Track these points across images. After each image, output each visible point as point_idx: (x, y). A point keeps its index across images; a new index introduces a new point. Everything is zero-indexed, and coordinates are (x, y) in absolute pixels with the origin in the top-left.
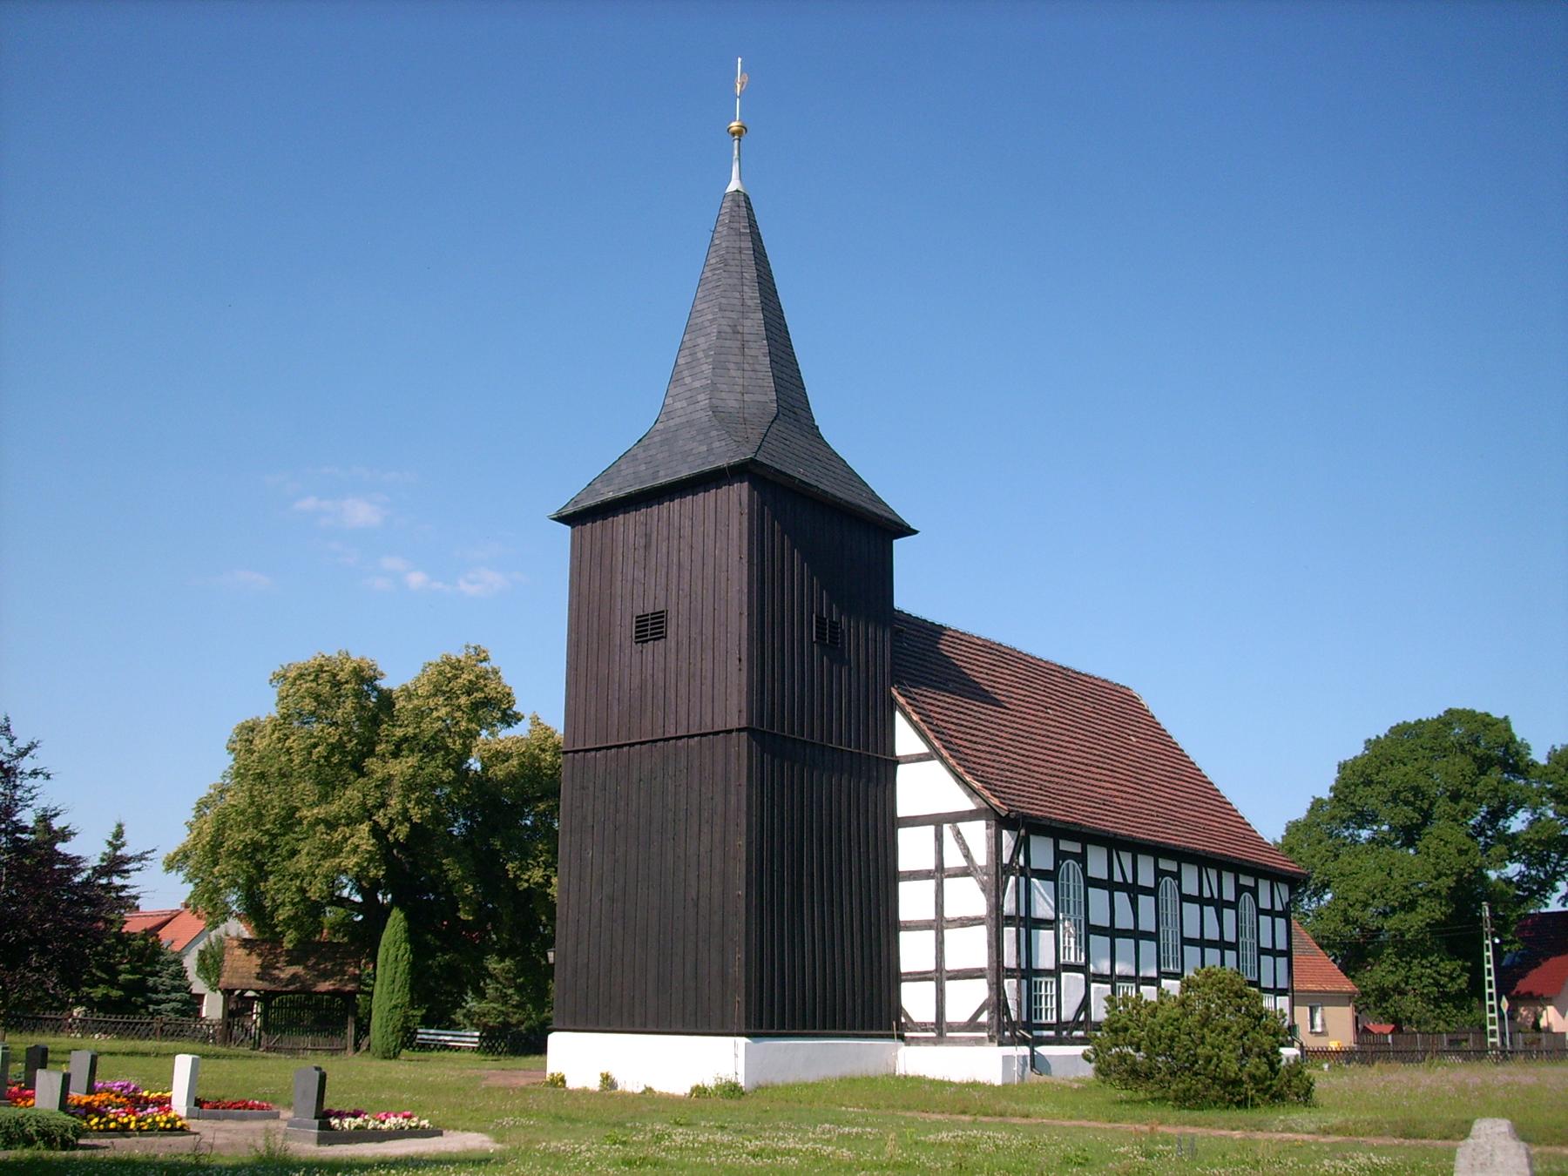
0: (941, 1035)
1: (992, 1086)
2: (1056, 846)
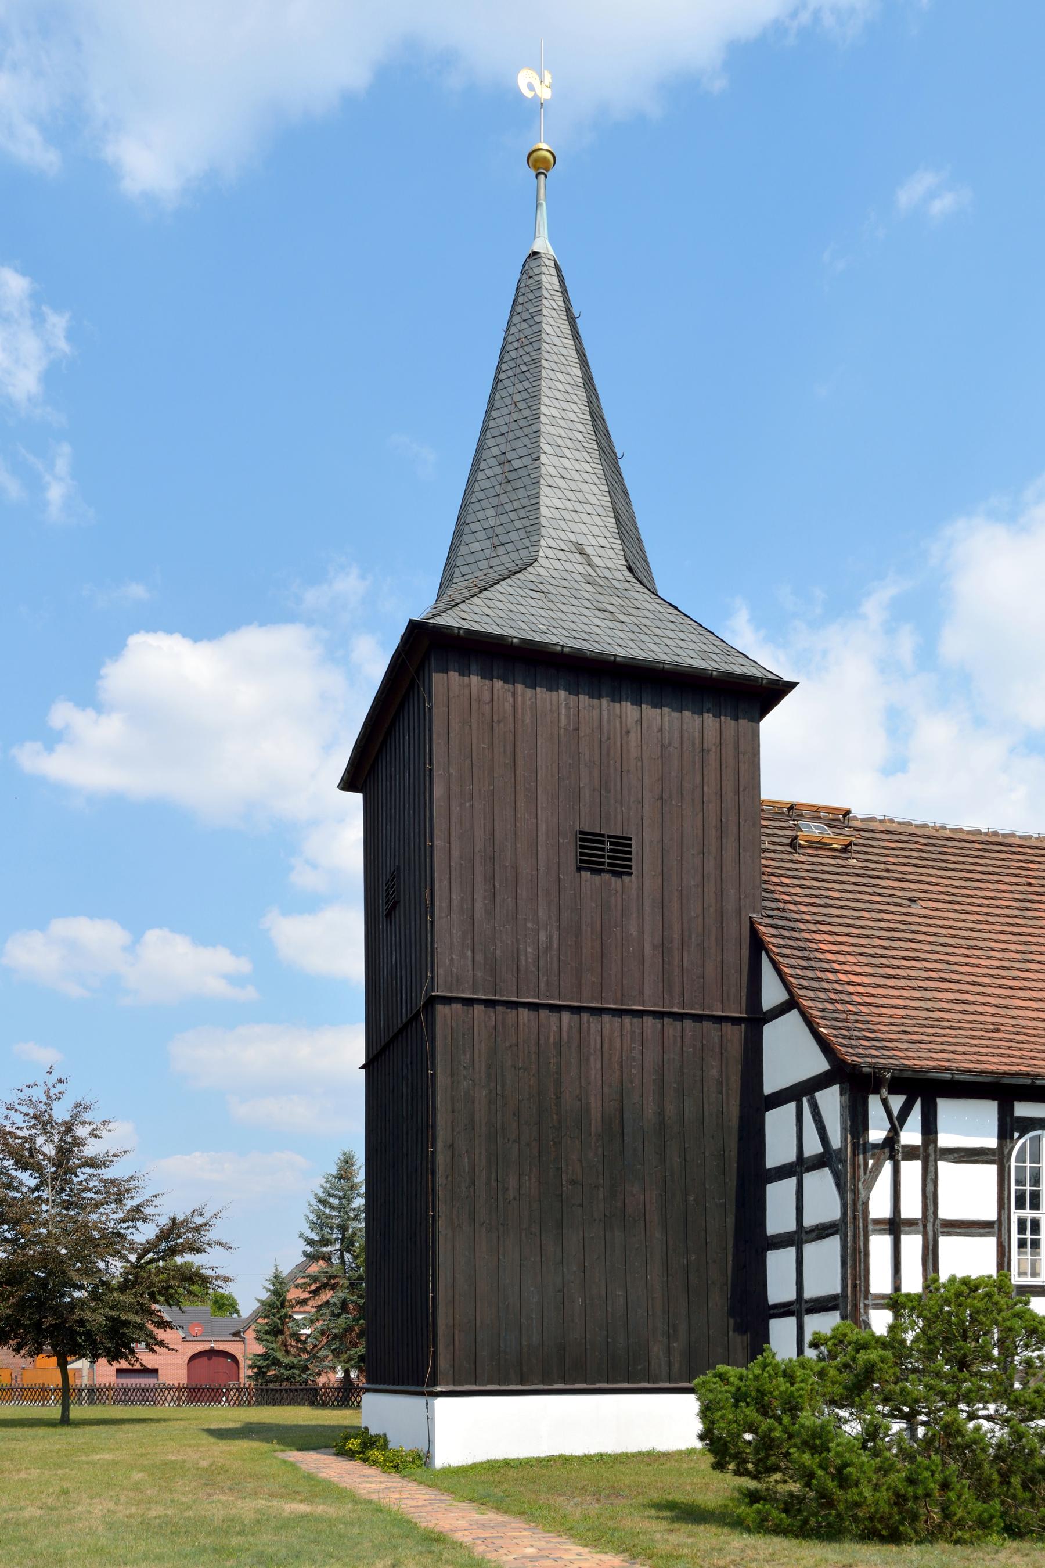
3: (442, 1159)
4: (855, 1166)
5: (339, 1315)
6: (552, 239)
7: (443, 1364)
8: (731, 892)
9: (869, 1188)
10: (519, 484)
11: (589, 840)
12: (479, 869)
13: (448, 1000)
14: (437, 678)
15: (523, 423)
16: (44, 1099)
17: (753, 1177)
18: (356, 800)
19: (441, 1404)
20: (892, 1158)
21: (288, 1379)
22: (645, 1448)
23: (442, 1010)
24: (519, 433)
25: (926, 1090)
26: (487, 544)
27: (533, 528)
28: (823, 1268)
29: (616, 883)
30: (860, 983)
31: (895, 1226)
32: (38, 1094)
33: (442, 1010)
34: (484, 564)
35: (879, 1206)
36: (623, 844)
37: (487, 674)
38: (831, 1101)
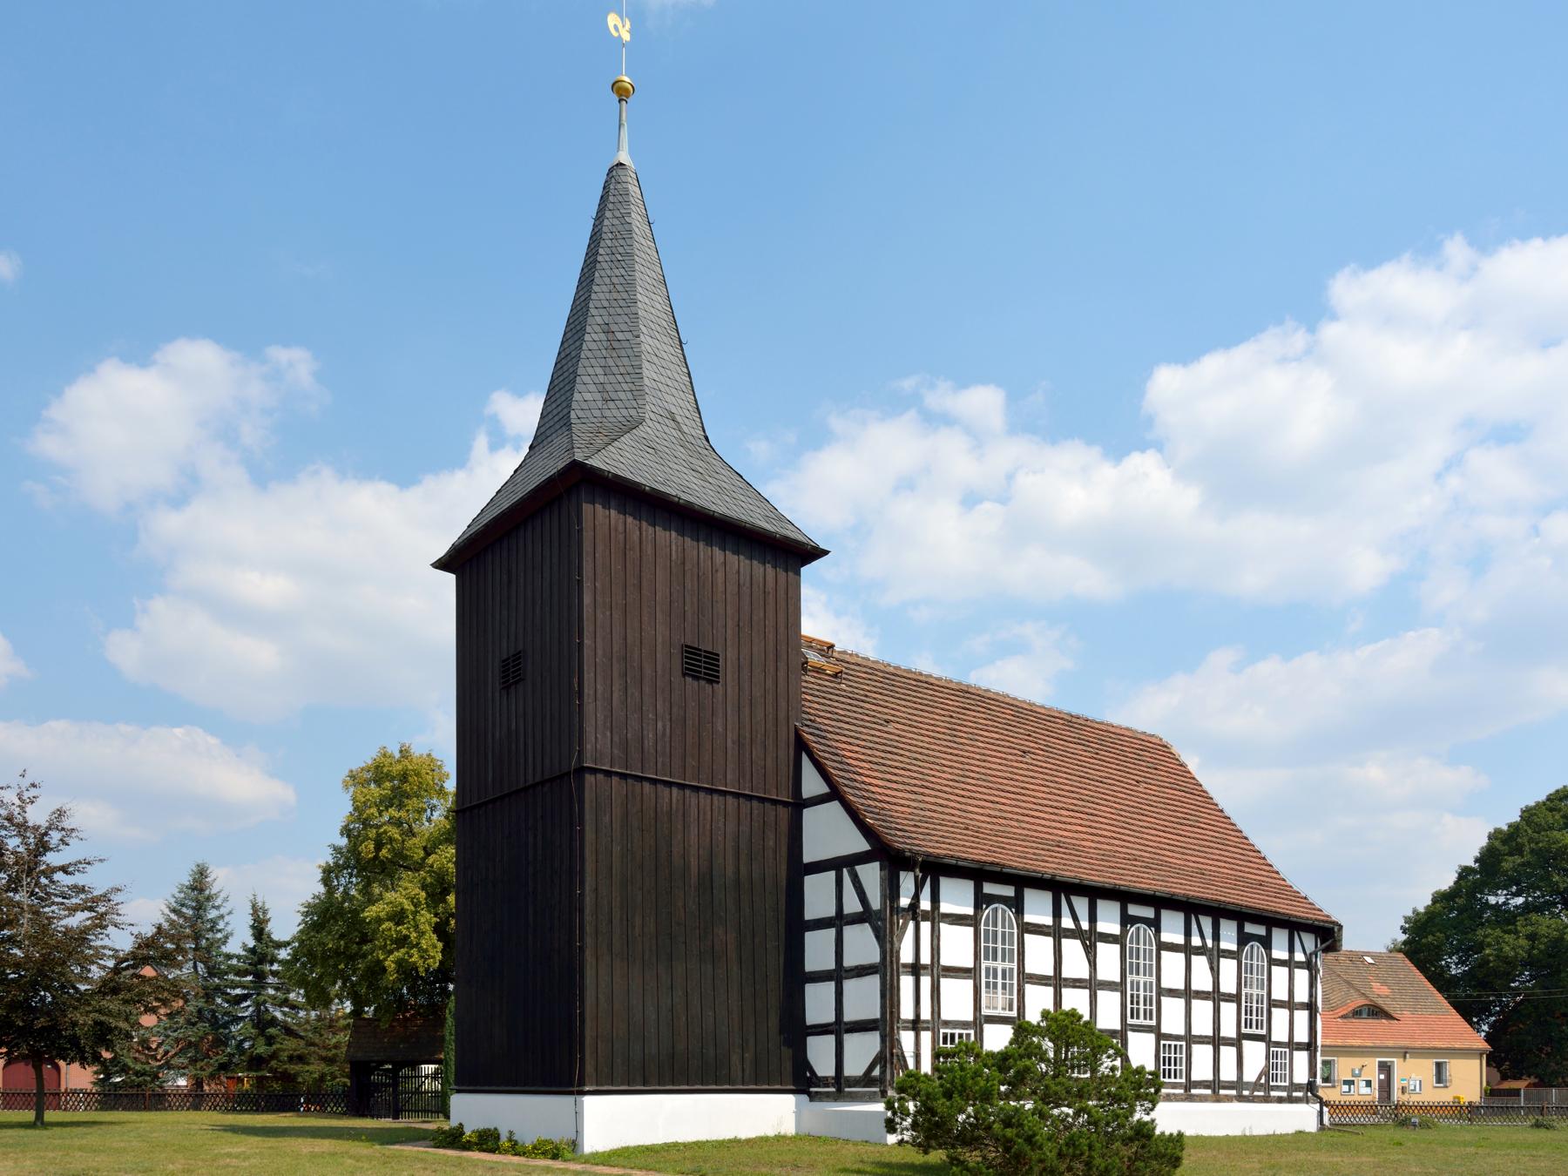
0: (839, 1090)
1: (780, 1138)
2: (1240, 929)
3: (589, 900)
5: (194, 1024)
6: (631, 153)
8: (783, 704)
9: (900, 941)
10: (623, 353)
11: (690, 652)
13: (594, 771)
15: (622, 303)
16: (18, 802)
17: (796, 926)
18: (450, 579)
19: (588, 1100)
20: (914, 918)
21: (139, 1086)
22: (729, 1135)
23: (589, 779)
24: (619, 311)
25: (935, 870)
26: (598, 396)
27: (638, 393)
28: (862, 999)
29: (708, 687)
31: (916, 969)
33: (589, 779)
35: (906, 956)
36: (713, 658)
37: (623, 511)
38: (871, 874)
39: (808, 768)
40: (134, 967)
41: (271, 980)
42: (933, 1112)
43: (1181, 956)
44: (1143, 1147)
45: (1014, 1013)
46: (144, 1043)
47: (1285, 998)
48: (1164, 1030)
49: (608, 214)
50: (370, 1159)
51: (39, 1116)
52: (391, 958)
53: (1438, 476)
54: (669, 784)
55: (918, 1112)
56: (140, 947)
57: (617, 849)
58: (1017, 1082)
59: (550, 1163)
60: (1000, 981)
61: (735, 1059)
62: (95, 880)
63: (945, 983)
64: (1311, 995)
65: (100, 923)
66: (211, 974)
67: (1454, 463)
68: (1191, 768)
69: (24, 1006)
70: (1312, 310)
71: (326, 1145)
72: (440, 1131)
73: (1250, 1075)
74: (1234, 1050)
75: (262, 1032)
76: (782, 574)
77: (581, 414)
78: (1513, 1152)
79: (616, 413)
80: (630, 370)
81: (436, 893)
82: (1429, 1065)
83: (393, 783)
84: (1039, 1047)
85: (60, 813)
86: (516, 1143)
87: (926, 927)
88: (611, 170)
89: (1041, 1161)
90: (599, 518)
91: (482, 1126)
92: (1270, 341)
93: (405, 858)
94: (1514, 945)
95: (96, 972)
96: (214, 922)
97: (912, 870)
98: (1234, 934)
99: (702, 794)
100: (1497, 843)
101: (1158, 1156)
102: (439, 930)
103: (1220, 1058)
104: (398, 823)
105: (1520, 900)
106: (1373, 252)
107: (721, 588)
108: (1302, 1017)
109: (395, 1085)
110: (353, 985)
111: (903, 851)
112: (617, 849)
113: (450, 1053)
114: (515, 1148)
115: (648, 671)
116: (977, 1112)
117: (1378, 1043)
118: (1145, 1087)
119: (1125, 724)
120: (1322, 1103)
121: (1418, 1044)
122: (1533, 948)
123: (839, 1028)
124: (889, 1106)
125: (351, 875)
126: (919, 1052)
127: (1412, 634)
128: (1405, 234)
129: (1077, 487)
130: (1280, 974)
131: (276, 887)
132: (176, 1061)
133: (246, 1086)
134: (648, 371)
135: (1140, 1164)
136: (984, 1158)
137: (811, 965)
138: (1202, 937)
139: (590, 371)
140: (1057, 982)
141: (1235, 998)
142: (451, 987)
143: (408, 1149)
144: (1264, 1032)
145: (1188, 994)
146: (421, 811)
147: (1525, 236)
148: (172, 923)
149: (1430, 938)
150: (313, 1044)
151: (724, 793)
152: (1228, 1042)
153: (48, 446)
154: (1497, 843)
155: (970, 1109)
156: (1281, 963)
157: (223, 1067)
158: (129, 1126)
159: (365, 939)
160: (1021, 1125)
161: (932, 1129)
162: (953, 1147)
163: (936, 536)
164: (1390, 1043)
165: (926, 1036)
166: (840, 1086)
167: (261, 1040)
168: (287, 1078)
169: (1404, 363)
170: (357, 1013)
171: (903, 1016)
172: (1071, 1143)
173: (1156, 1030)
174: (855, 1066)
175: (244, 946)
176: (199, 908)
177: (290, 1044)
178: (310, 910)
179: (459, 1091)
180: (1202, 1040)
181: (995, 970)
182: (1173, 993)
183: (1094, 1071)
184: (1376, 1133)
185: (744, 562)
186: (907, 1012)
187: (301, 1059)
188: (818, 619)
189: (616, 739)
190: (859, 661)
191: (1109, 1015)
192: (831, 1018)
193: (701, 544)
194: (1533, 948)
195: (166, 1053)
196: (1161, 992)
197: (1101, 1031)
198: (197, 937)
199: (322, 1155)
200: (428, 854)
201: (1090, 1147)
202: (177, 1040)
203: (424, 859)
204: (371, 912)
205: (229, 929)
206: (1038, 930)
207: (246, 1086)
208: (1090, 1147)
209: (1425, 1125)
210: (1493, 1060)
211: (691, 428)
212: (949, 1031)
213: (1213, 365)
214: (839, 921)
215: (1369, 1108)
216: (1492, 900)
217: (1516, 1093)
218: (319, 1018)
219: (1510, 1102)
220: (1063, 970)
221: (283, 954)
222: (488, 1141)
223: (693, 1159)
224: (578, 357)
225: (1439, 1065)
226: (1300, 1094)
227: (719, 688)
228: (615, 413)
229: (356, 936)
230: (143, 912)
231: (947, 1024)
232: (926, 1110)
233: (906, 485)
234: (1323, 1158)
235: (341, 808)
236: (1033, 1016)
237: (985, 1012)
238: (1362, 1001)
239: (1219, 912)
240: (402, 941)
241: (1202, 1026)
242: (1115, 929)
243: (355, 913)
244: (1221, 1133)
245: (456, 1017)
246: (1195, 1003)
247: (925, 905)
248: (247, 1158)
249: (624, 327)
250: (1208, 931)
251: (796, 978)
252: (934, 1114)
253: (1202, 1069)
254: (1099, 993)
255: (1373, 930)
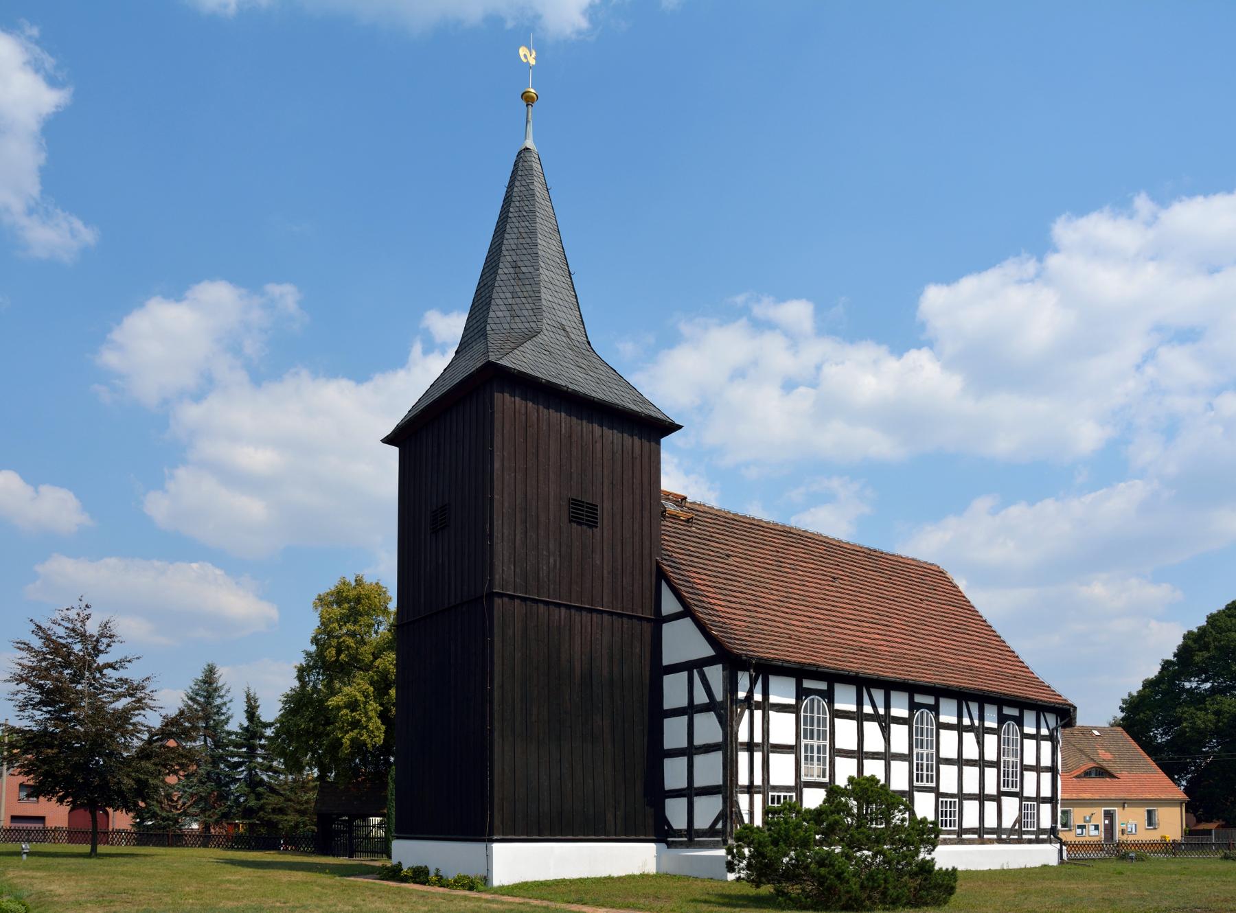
0: (691, 840)
1: (644, 876)
4: (732, 712)
5: (204, 783)
7: (497, 822)
8: (647, 543)
11: (575, 504)
12: (518, 515)
14: (498, 396)
17: (657, 714)
18: (394, 451)
19: (496, 846)
21: (164, 828)
23: (498, 601)
25: (765, 670)
26: (507, 314)
27: (537, 310)
28: (709, 770)
29: (589, 531)
30: (720, 605)
31: (750, 747)
32: (72, 614)
33: (498, 601)
34: (507, 326)
35: (743, 736)
36: (593, 508)
38: (715, 674)
39: (667, 594)
40: (161, 740)
41: (260, 751)
42: (763, 856)
43: (955, 733)
44: (925, 880)
45: (827, 780)
46: (169, 797)
47: (1034, 763)
48: (942, 790)
49: (517, 183)
50: (332, 887)
51: (94, 849)
52: (347, 736)
53: (1138, 367)
54: (559, 605)
55: (752, 856)
56: (167, 725)
57: (518, 655)
58: (828, 833)
59: (467, 893)
60: (815, 755)
61: (610, 816)
62: (133, 673)
63: (774, 757)
64: (1053, 761)
65: (140, 704)
66: (217, 747)
67: (1149, 357)
68: (961, 588)
69: (83, 768)
70: (1042, 246)
71: (299, 876)
72: (384, 868)
73: (1007, 823)
74: (994, 804)
75: (253, 791)
76: (646, 444)
77: (494, 327)
78: (1208, 878)
79: (520, 325)
80: (532, 294)
81: (381, 686)
82: (1141, 812)
83: (349, 604)
84: (846, 804)
85: (105, 625)
86: (442, 877)
87: (758, 714)
88: (520, 153)
89: (848, 892)
90: (507, 403)
91: (415, 864)
92: (1010, 268)
93: (358, 661)
94: (1204, 719)
95: (136, 743)
96: (219, 707)
97: (748, 670)
98: (995, 716)
99: (584, 613)
100: (1190, 642)
101: (937, 886)
102: (383, 716)
103: (984, 807)
104: (353, 635)
105: (1208, 685)
106: (1083, 205)
107: (599, 455)
108: (1046, 778)
109: (351, 832)
110: (320, 756)
111: (741, 655)
112: (518, 655)
113: (392, 808)
114: (441, 882)
115: (543, 519)
116: (797, 856)
117: (1103, 796)
118: (928, 834)
119: (911, 556)
120: (1062, 843)
121: (1134, 796)
122: (1218, 721)
123: (690, 792)
124: (729, 851)
125: (318, 674)
126: (751, 809)
127: (1122, 484)
128: (1108, 192)
129: (869, 376)
130: (1030, 745)
131: (264, 682)
132: (192, 810)
133: (241, 830)
134: (545, 295)
135: (924, 893)
136: (803, 890)
137: (668, 744)
138: (971, 718)
139: (502, 295)
140: (860, 755)
141: (996, 765)
142: (392, 759)
143: (360, 880)
144: (1018, 790)
145: (960, 762)
146: (370, 626)
147: (1191, 193)
148: (189, 707)
149: (1142, 715)
150: (290, 800)
151: (602, 612)
152: (991, 798)
153: (110, 358)
154: (1190, 642)
155: (792, 853)
156: (1030, 737)
157: (225, 816)
158: (156, 858)
159: (328, 722)
160: (833, 865)
161: (762, 869)
162: (779, 882)
163: (757, 413)
164: (1113, 796)
165: (758, 798)
166: (691, 837)
167: (252, 796)
168: (272, 825)
169: (1110, 284)
170: (322, 777)
171: (740, 783)
172: (871, 877)
173: (936, 790)
174: (703, 821)
175: (241, 726)
176: (209, 697)
177: (273, 799)
178: (289, 699)
179: (398, 838)
180: (971, 797)
181: (812, 747)
182: (948, 761)
183: (888, 822)
184: (1103, 865)
185: (617, 435)
186: (743, 780)
187: (281, 811)
188: (676, 476)
189: (518, 570)
190: (706, 509)
191: (899, 782)
192: (684, 785)
193: (584, 422)
194: (1218, 721)
195: (184, 804)
196: (940, 761)
197: (894, 792)
198: (207, 718)
199: (297, 883)
200: (375, 658)
201: (886, 881)
202: (192, 795)
203: (372, 662)
204: (333, 702)
205: (230, 713)
206: (845, 715)
207: (241, 830)
208: (886, 881)
209: (1140, 858)
210: (1190, 808)
211: (576, 336)
212: (776, 794)
213: (969, 285)
214: (690, 710)
215: (1097, 846)
216: (1187, 685)
217: (1209, 832)
218: (294, 781)
219: (1204, 839)
220: (867, 746)
221: (269, 732)
222: (420, 875)
223: (577, 891)
224: (493, 286)
225: (1149, 812)
226: (1045, 837)
227: (597, 531)
228: (520, 326)
229: (322, 720)
230: (169, 699)
231: (775, 788)
232: (758, 854)
233: (739, 374)
234: (1063, 885)
235: (311, 623)
236: (841, 781)
237: (804, 779)
238: (1091, 765)
239: (983, 699)
240: (355, 724)
241: (971, 786)
242: (904, 713)
243: (321, 702)
244: (986, 868)
245: (396, 782)
246: (966, 769)
247: (758, 697)
248: (242, 884)
249: (528, 263)
250: (975, 713)
251: (657, 754)
252: (764, 857)
253: (970, 817)
254: (892, 763)
255: (1099, 709)
